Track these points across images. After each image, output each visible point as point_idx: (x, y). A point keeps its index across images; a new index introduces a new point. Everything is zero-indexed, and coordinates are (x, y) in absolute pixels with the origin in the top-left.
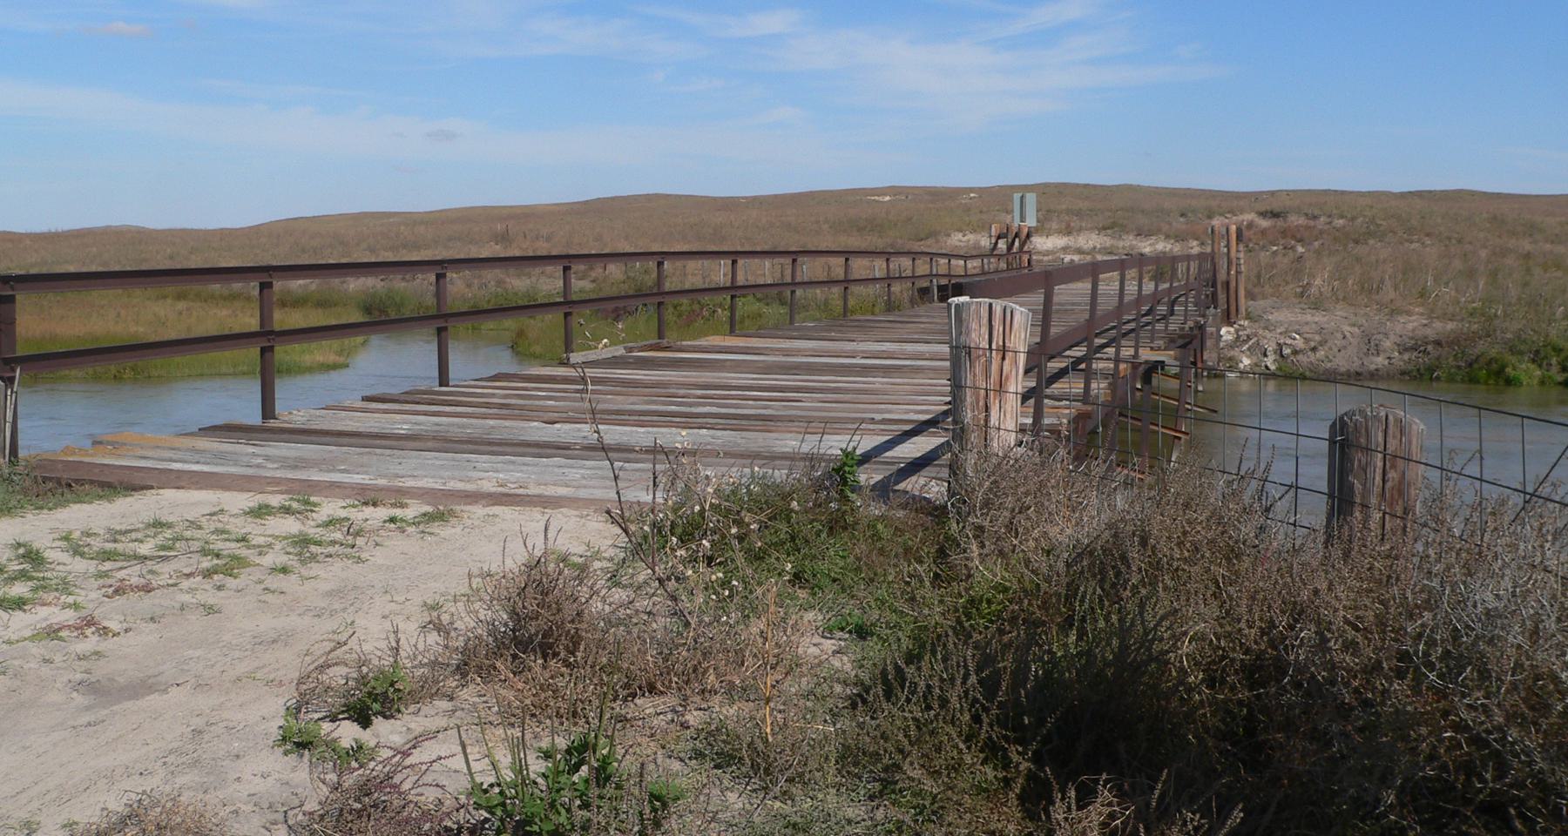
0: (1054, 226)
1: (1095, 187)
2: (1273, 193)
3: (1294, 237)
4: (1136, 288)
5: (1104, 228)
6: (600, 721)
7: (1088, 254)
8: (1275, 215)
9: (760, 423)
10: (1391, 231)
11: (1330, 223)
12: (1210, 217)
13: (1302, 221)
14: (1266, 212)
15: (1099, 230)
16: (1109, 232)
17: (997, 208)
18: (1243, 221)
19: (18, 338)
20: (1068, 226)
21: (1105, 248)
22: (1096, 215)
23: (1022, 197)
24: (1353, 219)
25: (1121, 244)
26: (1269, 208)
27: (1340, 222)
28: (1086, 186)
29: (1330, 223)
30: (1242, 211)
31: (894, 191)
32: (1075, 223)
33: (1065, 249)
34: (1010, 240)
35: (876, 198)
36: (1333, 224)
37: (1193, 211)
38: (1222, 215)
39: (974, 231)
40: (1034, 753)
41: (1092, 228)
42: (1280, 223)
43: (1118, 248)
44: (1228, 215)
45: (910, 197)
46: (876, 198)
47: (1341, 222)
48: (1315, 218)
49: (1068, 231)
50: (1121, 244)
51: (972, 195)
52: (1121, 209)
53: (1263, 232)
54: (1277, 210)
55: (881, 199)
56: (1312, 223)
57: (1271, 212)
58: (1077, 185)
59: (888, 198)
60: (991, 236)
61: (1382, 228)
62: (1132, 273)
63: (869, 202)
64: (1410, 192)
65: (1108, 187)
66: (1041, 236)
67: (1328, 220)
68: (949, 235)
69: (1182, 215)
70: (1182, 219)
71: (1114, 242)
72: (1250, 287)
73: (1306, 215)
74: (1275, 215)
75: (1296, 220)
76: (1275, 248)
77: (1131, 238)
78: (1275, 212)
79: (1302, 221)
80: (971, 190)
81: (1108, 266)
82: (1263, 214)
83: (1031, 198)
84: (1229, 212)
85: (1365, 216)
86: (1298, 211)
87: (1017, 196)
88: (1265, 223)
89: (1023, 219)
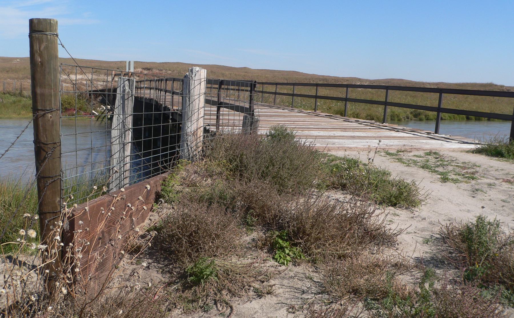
4: (31, 102)
6: (63, 223)
8: (148, 69)
13: (157, 71)
14: (145, 68)
18: (139, 71)
19: (31, 79)
24: (173, 71)
26: (146, 67)
27: (170, 72)
40: (150, 252)
41: (89, 72)
42: (151, 72)
43: (99, 79)
47: (170, 72)
48: (161, 70)
50: (100, 78)
51: (18, 60)
54: (149, 68)
56: (161, 72)
57: (147, 68)
65: (65, 59)
67: (166, 71)
72: (62, 102)
74: (148, 69)
77: (103, 76)
79: (157, 71)
80: (17, 58)
81: (170, 79)
82: (144, 69)
85: (177, 70)
86: (156, 68)
88: (146, 72)
89: (129, 69)
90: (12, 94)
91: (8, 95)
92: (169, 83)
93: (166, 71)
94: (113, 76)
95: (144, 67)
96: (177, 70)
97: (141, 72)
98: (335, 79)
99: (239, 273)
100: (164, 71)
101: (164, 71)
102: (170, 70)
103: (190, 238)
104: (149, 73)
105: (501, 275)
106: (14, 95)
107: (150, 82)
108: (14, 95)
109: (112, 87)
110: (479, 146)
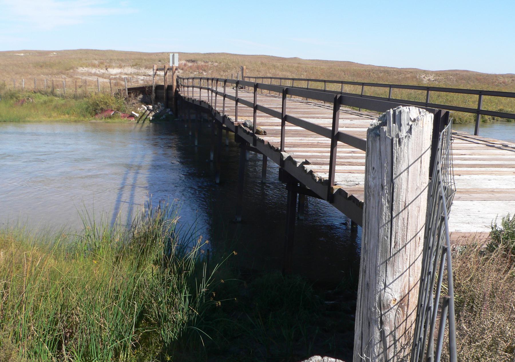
0: (114, 65)
1: (99, 50)
2: (163, 53)
3: (201, 69)
5: (133, 66)
7: (130, 75)
8: (193, 61)
9: (444, 144)
10: (235, 67)
11: (213, 64)
13: (203, 63)
15: (131, 66)
16: (135, 67)
17: (91, 58)
18: (182, 63)
20: (120, 65)
21: (135, 73)
22: (128, 61)
23: (173, 55)
24: (220, 63)
25: (140, 71)
27: (216, 64)
28: (95, 50)
29: (213, 64)
31: (25, 52)
32: (123, 64)
33: (121, 73)
34: (166, 71)
35: (18, 54)
36: (214, 65)
37: (163, 60)
39: (86, 67)
41: (128, 66)
42: (195, 64)
45: (31, 54)
46: (18, 54)
47: (216, 64)
48: (207, 62)
49: (120, 67)
51: (55, 53)
52: (137, 59)
53: (191, 67)
54: (193, 59)
55: (19, 54)
56: (207, 64)
57: (191, 60)
58: (92, 50)
59: (22, 54)
60: (153, 70)
61: (231, 66)
62: (210, 81)
63: (16, 55)
64: (207, 53)
65: (104, 51)
66: (111, 68)
68: (77, 68)
69: (160, 61)
70: (160, 63)
71: (138, 71)
73: (204, 61)
74: (193, 61)
75: (201, 63)
76: (195, 73)
77: (144, 69)
78: (193, 60)
79: (203, 63)
83: (177, 56)
85: (224, 62)
86: (201, 60)
87: (171, 55)
88: (190, 64)
89: (173, 63)
90: (43, 93)
91: (39, 94)
93: (212, 63)
95: (188, 59)
96: (224, 62)
97: (185, 65)
98: (397, 71)
100: (210, 63)
101: (210, 63)
102: (216, 62)
104: (193, 65)
106: (46, 94)
108: (46, 94)
109: (154, 83)
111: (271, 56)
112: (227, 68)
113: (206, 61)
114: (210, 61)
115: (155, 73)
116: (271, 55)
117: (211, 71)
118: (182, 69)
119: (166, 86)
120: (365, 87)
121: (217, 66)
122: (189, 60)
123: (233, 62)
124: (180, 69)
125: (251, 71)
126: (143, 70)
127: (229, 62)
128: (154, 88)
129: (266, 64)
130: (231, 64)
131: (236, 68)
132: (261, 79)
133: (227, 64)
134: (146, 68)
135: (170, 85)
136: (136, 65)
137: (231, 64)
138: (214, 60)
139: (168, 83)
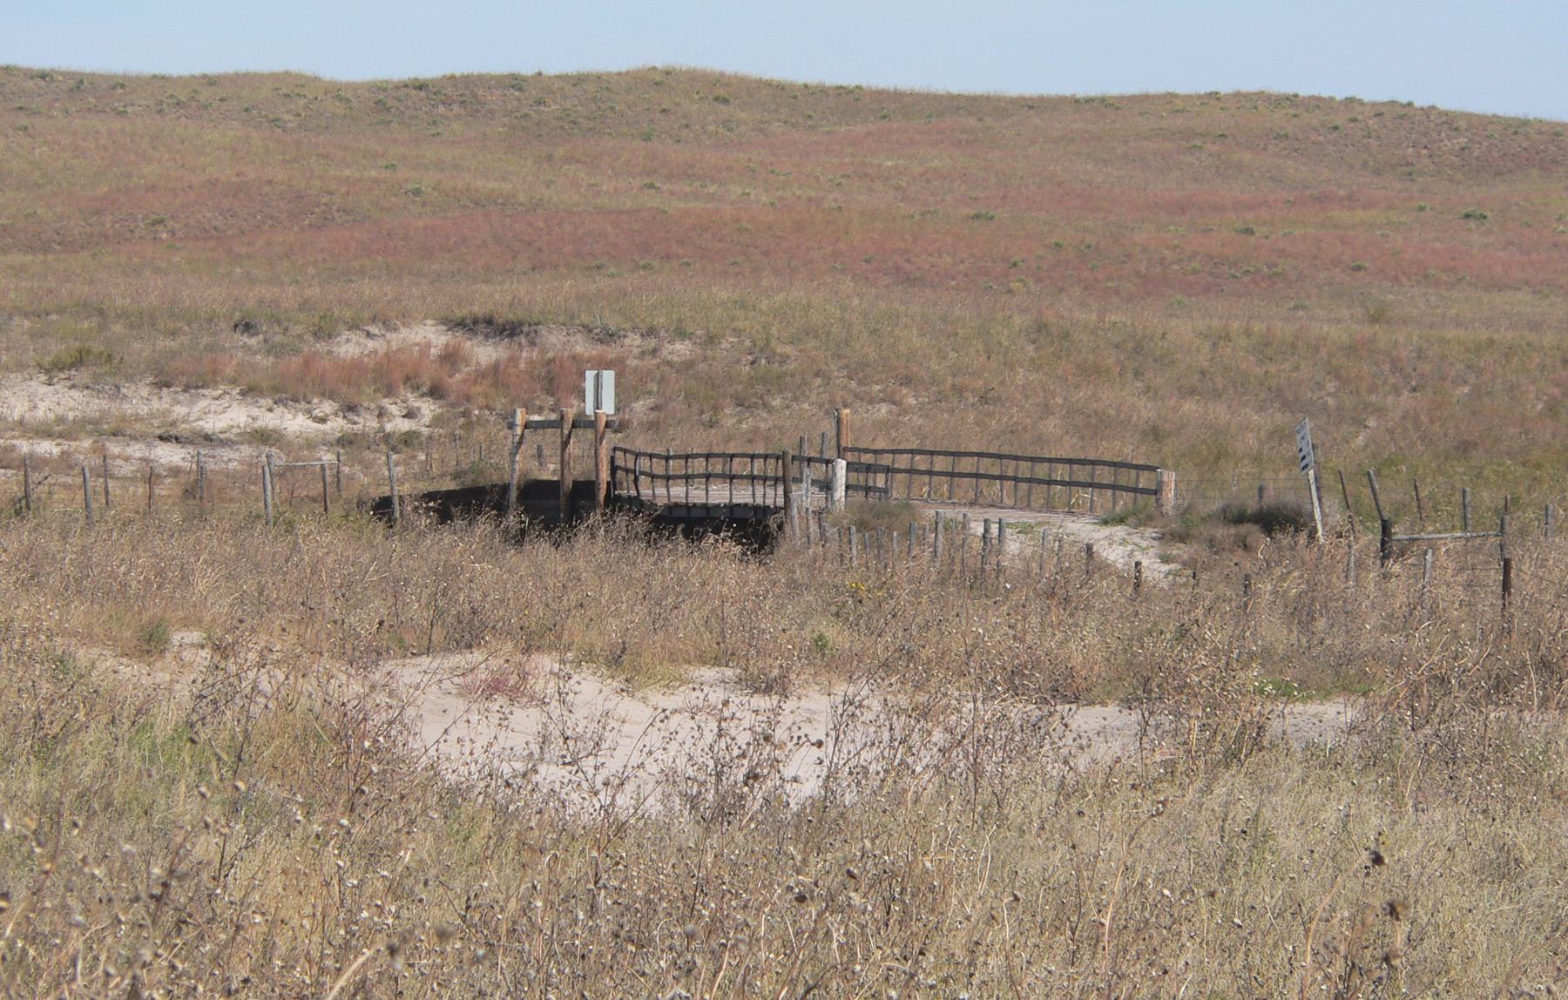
8: (508, 330)
10: (817, 375)
11: (654, 352)
12: (324, 332)
23: (598, 374)
24: (711, 340)
26: (478, 310)
27: (681, 349)
30: (406, 318)
34: (566, 432)
38: (354, 326)
44: (373, 330)
47: (681, 349)
57: (489, 322)
64: (421, 86)
69: (248, 328)
77: (145, 392)
84: (374, 320)
85: (737, 332)
86: (569, 322)
88: (485, 353)
89: (598, 406)
92: (758, 463)
93: (652, 343)
94: (519, 431)
95: (459, 313)
96: (737, 332)
97: (450, 358)
99: (681, 921)
100: (633, 341)
101: (633, 341)
102: (681, 334)
103: (535, 851)
104: (513, 360)
105: (878, 387)
107: (686, 462)
109: (516, 476)
110: (811, 522)
111: (1379, 111)
112: (764, 380)
113: (605, 329)
114: (634, 329)
115: (517, 439)
116: (1374, 91)
117: (651, 401)
118: (435, 392)
119: (569, 483)
120: (935, 457)
121: (689, 365)
122: (476, 322)
123: (809, 331)
124: (415, 388)
125: (940, 398)
126: (141, 401)
127: (774, 331)
128: (514, 494)
129: (1066, 336)
130: (788, 349)
131: (828, 379)
132: (937, 468)
133: (762, 350)
134: (162, 384)
135: (581, 479)
136: (79, 361)
137: (788, 349)
138: (661, 320)
139: (577, 472)
